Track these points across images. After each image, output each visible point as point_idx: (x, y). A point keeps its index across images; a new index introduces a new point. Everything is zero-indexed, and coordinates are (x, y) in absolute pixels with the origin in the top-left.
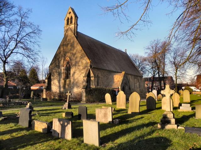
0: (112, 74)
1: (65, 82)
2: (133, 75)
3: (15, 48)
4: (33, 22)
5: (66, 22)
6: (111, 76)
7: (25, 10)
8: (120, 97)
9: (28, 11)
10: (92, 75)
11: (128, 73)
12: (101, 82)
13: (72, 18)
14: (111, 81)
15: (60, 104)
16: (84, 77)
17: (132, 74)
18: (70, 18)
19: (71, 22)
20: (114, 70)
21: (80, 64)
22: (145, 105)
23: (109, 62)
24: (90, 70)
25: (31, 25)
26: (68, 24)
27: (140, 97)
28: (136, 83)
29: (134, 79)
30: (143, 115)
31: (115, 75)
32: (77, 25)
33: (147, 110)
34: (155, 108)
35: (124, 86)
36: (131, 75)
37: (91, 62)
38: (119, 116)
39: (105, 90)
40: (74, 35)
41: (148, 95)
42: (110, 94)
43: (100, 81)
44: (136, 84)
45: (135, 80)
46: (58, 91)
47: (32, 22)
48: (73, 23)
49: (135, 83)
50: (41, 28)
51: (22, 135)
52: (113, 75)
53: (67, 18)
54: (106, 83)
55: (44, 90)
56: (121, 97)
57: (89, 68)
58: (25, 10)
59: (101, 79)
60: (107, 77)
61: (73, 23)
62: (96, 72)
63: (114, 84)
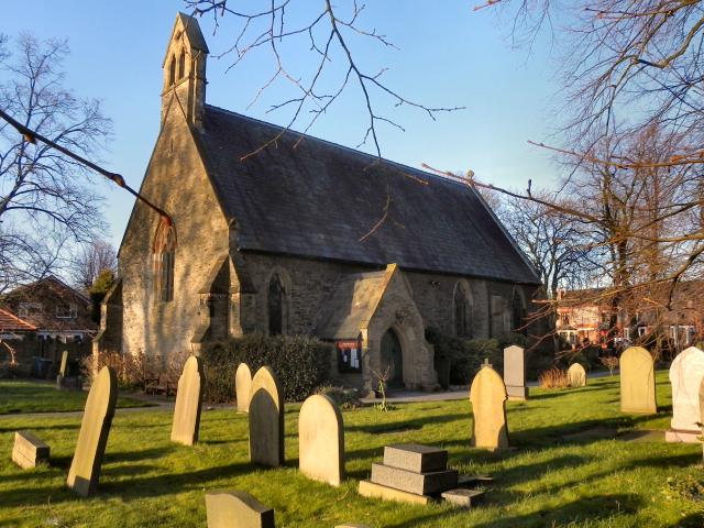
0: (350, 276)
1: (161, 310)
2: (480, 278)
4: (72, 90)
5: (166, 72)
8: (185, 385)
10: (235, 282)
11: (456, 271)
12: (292, 311)
14: (339, 308)
15: (458, 387)
16: (201, 292)
17: (476, 273)
18: (177, 57)
19: (181, 75)
20: (368, 260)
21: (204, 232)
22: (289, 435)
23: (347, 227)
24: (227, 258)
26: (172, 80)
27: (474, 376)
28: (497, 314)
29: (489, 294)
31: (361, 279)
32: (203, 81)
34: (275, 457)
35: (391, 331)
36: (470, 277)
37: (237, 225)
39: (279, 348)
40: (186, 124)
41: (147, 387)
43: (288, 307)
44: (495, 318)
48: (187, 74)
49: (493, 311)
50: (105, 111)
51: (40, 507)
52: (355, 280)
53: (169, 60)
54: (320, 317)
55: (95, 347)
58: (43, 49)
59: (289, 297)
61: (187, 74)
63: (349, 317)
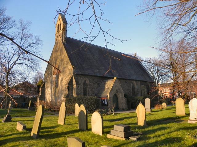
1: (55, 90)
3: (17, 60)
5: (57, 29)
6: (103, 83)
7: (25, 23)
9: (80, 19)
10: (74, 82)
13: (61, 24)
15: (133, 109)
16: (66, 85)
17: (137, 79)
19: (60, 29)
25: (31, 36)
26: (58, 31)
28: (143, 90)
29: (141, 85)
30: (2, 139)
33: (79, 129)
34: (85, 129)
38: (8, 138)
39: (86, 99)
42: (78, 104)
44: (142, 91)
45: (142, 86)
46: (102, 96)
47: (31, 32)
49: (142, 89)
50: (41, 39)
52: (106, 81)
53: (57, 25)
54: (97, 91)
56: (63, 110)
57: (72, 74)
58: (25, 23)
60: (98, 84)
61: (62, 29)
62: (82, 79)
63: (104, 91)
